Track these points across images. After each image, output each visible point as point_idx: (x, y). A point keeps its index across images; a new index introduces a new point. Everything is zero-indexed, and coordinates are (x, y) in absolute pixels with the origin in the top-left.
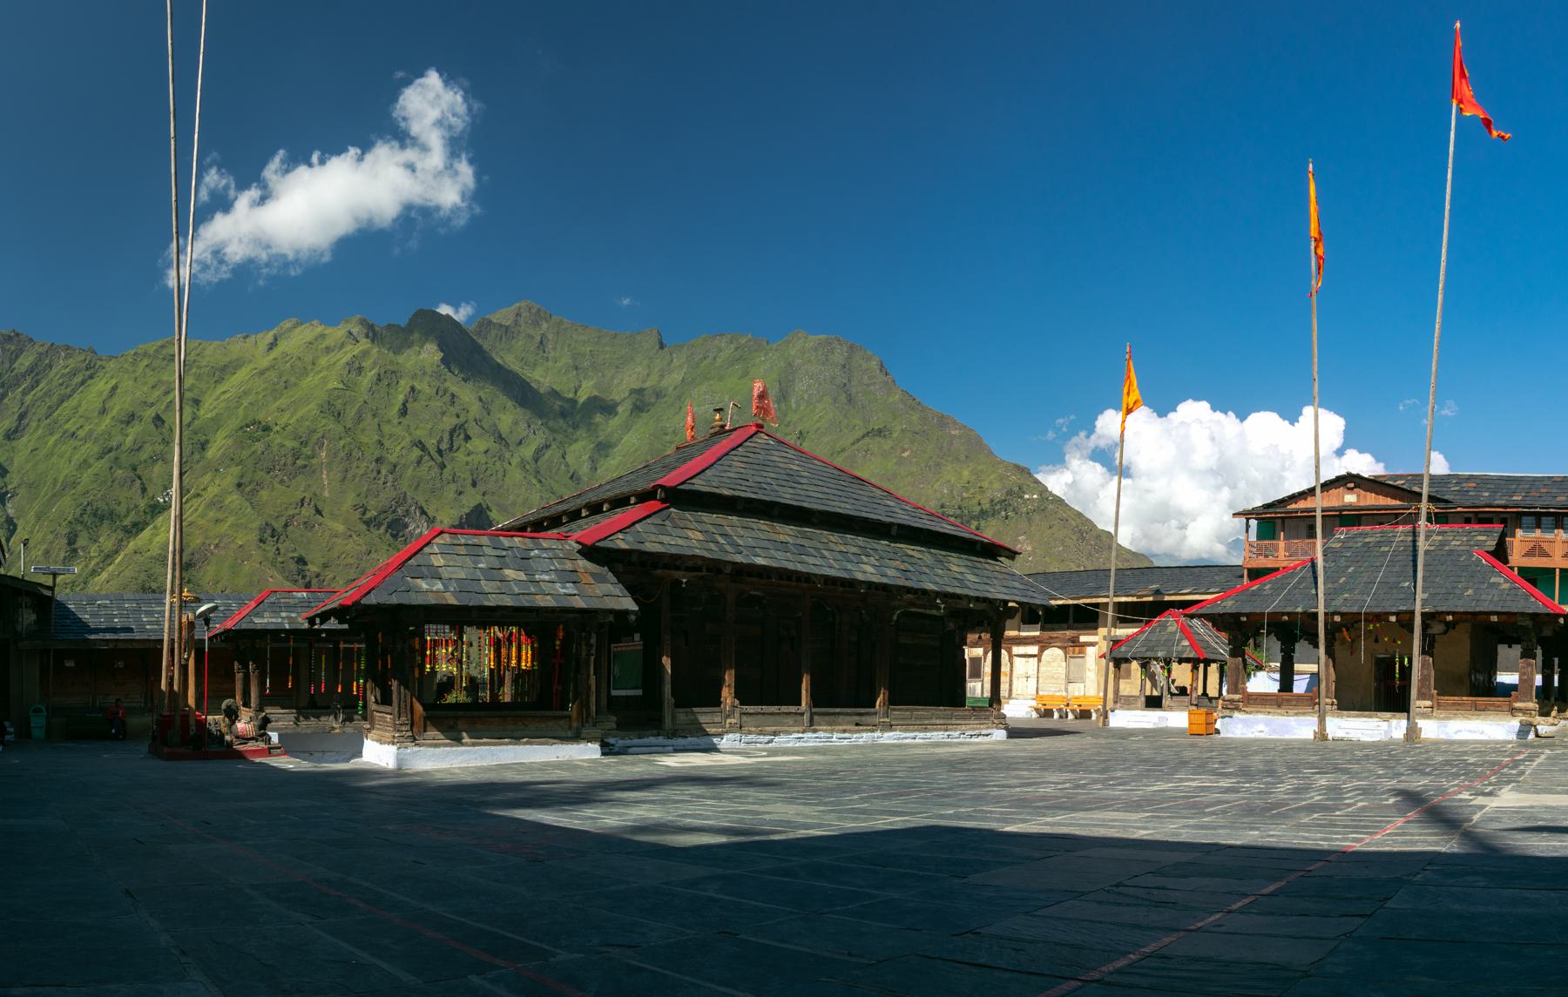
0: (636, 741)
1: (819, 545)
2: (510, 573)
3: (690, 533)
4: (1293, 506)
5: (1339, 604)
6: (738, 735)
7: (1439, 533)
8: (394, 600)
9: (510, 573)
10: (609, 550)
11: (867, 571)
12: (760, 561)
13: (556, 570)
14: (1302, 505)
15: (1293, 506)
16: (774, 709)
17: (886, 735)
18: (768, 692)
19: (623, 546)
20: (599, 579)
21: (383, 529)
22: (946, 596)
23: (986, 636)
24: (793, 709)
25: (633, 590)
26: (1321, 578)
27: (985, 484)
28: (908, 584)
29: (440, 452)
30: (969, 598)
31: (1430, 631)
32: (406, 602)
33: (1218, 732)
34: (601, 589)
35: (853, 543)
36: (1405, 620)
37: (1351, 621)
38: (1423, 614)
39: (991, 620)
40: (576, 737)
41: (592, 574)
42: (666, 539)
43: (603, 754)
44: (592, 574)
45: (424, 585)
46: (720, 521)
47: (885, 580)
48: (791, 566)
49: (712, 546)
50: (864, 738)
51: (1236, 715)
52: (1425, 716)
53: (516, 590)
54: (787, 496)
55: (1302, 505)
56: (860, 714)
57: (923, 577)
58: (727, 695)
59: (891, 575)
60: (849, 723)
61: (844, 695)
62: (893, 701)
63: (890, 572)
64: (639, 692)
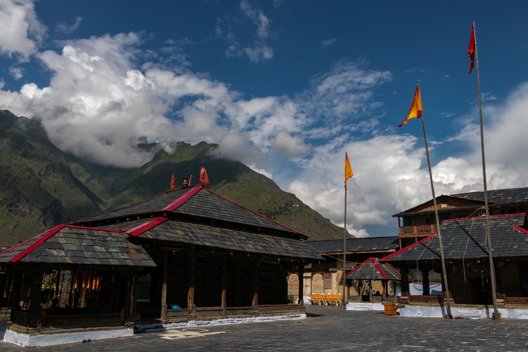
0: (149, 326)
1: (230, 237)
2: (97, 248)
3: (178, 231)
4: (425, 210)
5: (450, 255)
6: (194, 321)
7: (493, 220)
8: (39, 260)
9: (97, 248)
10: (143, 238)
11: (250, 247)
12: (207, 244)
13: (119, 247)
14: (429, 209)
15: (425, 210)
16: (210, 308)
17: (257, 318)
18: (207, 301)
19: (150, 237)
20: (138, 251)
21: (5, 207)
22: (281, 257)
23: (293, 279)
24: (218, 308)
25: (153, 256)
26: (441, 241)
27: (277, 201)
28: (266, 252)
29: (40, 175)
30: (290, 257)
31: (497, 266)
32: (46, 261)
33: (398, 314)
34: (142, 256)
35: (243, 235)
36: (485, 261)
37: (458, 263)
38: (493, 258)
39: (300, 266)
40: (122, 324)
41: (135, 249)
42: (168, 234)
43: (135, 333)
44: (135, 249)
45: (55, 253)
46: (189, 226)
47: (257, 251)
48: (220, 246)
49: (187, 237)
50: (247, 320)
51: (407, 306)
52: (501, 307)
53: (101, 256)
54: (216, 216)
55: (429, 209)
56: (246, 309)
57: (272, 249)
58: (191, 304)
59: (259, 249)
60: (241, 313)
61: (239, 303)
62: (261, 302)
63: (259, 248)
64: (148, 301)
